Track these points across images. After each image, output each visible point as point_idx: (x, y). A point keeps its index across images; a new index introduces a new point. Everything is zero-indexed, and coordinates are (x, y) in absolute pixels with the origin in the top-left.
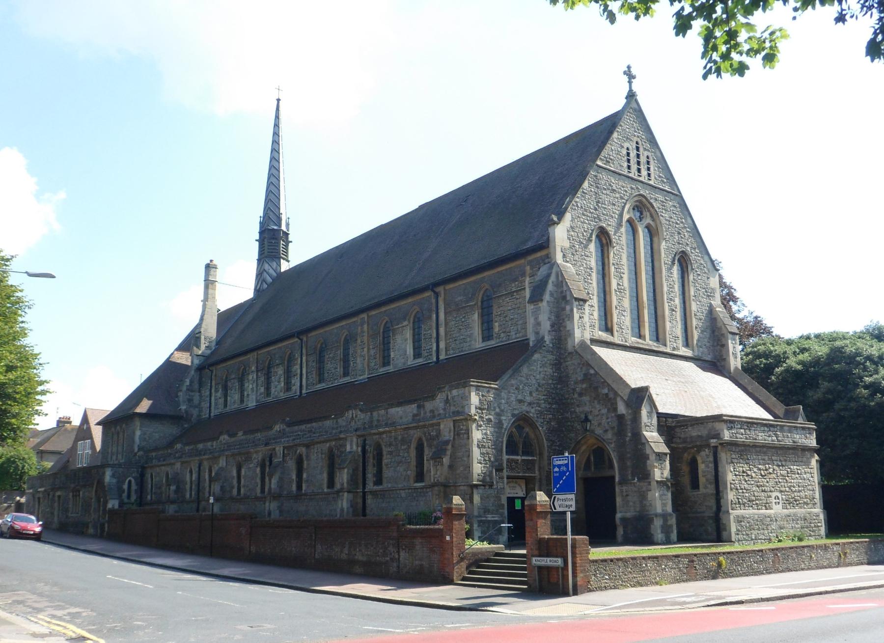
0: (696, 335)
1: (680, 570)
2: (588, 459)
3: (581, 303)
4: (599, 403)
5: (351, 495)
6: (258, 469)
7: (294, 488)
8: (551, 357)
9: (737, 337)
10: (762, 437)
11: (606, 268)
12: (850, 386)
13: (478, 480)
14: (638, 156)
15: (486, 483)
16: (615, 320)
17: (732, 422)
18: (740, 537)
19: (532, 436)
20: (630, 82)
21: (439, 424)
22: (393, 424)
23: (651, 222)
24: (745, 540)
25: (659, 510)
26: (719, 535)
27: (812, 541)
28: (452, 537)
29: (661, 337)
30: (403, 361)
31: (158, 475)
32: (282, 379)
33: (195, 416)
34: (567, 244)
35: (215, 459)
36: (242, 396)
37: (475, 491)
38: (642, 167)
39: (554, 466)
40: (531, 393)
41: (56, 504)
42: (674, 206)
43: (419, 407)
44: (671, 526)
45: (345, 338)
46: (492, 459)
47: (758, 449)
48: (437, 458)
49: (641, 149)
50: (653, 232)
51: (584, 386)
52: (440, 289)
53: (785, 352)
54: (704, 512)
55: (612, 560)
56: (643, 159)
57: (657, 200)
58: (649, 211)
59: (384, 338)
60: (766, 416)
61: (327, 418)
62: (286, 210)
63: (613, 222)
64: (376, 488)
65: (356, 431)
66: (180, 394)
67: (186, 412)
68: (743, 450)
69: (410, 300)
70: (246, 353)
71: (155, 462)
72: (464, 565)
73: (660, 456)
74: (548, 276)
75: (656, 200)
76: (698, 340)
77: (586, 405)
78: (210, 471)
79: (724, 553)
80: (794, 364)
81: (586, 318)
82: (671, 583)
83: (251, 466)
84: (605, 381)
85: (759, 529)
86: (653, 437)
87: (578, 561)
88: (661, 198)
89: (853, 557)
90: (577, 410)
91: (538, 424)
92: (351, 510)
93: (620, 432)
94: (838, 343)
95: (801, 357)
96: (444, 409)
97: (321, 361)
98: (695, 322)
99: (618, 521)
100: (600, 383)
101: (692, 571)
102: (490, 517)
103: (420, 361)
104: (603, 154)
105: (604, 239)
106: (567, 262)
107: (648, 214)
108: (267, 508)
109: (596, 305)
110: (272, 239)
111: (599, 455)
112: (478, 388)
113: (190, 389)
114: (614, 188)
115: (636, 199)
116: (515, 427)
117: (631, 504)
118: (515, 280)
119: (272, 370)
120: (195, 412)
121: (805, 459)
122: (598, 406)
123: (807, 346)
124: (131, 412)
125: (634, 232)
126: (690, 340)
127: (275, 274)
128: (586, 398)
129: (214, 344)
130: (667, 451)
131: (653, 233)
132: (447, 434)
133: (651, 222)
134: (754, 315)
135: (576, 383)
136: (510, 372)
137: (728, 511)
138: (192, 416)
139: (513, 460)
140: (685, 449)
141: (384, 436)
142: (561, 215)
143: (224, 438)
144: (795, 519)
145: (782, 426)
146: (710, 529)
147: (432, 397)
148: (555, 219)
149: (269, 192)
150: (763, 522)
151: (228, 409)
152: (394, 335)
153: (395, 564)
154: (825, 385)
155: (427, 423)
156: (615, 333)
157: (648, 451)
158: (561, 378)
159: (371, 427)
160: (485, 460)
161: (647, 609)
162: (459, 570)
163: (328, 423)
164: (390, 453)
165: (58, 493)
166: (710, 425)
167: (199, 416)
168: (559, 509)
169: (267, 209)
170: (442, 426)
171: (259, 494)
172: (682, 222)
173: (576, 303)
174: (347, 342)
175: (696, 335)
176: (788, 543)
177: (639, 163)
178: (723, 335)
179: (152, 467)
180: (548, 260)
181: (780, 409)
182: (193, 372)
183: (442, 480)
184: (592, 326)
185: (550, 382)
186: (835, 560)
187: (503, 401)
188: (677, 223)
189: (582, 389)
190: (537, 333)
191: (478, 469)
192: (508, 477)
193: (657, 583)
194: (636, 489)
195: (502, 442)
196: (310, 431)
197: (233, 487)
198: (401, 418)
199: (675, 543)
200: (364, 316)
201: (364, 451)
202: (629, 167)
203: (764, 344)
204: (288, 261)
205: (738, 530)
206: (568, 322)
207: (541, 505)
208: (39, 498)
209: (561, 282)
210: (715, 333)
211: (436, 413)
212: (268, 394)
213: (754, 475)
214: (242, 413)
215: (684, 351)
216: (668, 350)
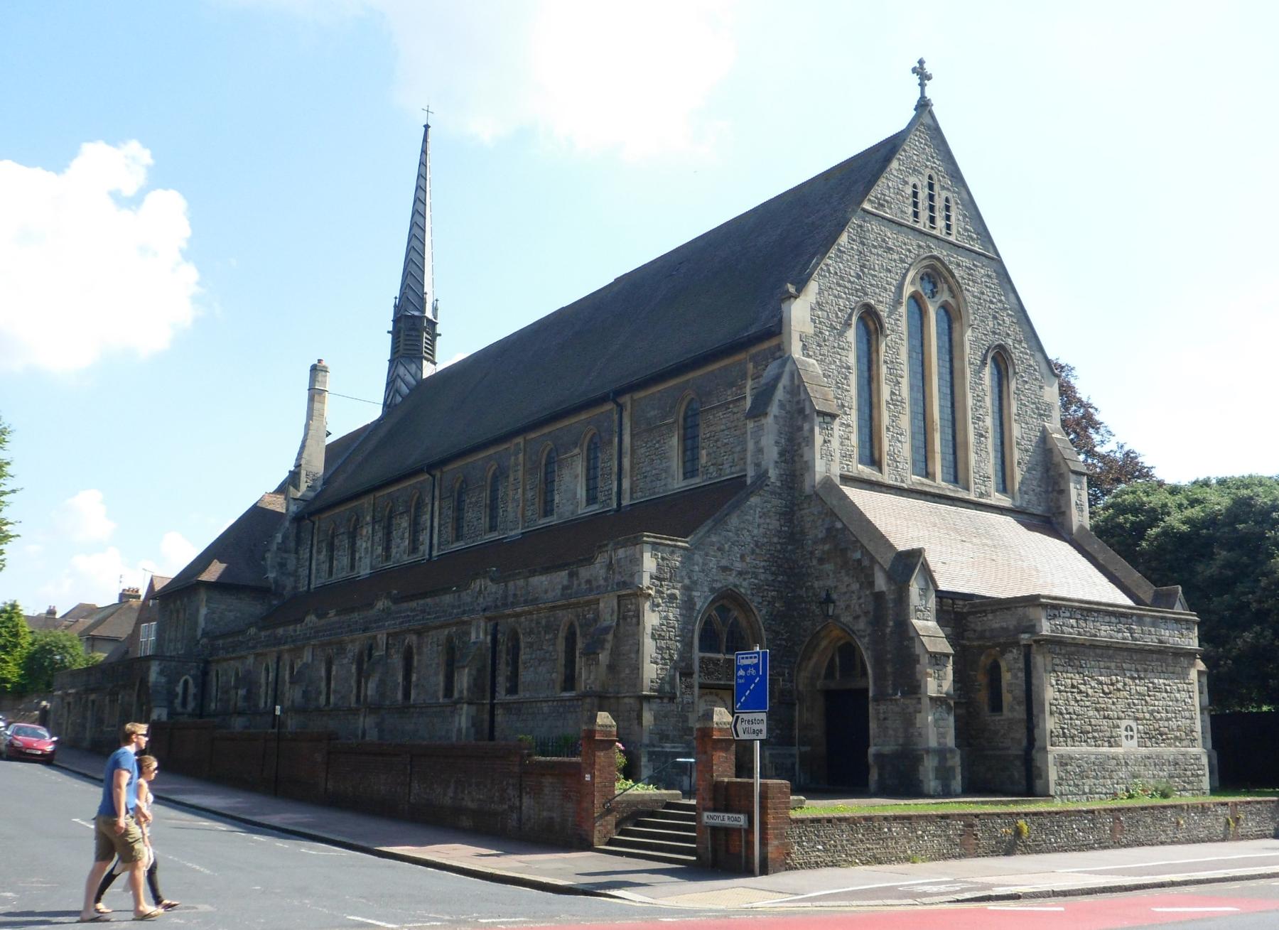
0: (1018, 475)
1: (948, 838)
2: (832, 659)
3: (828, 419)
4: (848, 574)
5: (474, 708)
6: (354, 667)
7: (400, 696)
8: (776, 502)
9: (1085, 479)
10: (1105, 632)
11: (874, 367)
12: (1261, 557)
13: (651, 689)
14: (931, 197)
15: (664, 694)
17: (1055, 607)
18: (1065, 788)
19: (743, 622)
20: (922, 85)
21: (597, 602)
22: (535, 601)
23: (950, 300)
24: (1072, 793)
25: (933, 743)
26: (1029, 783)
27: (1187, 799)
28: (593, 777)
29: (961, 475)
30: (571, 507)
31: (226, 671)
32: (407, 535)
33: (289, 588)
34: (810, 329)
35: (297, 651)
36: (353, 559)
37: (645, 706)
38: (937, 214)
39: (739, 667)
40: (742, 557)
41: (89, 714)
42: (989, 276)
43: (571, 575)
44: (952, 769)
45: (494, 473)
46: (675, 657)
47: (1098, 651)
48: (591, 652)
49: (937, 187)
50: (952, 316)
51: (827, 547)
52: (626, 399)
53: (1165, 505)
54: (1008, 748)
55: (829, 821)
56: (939, 203)
57: (959, 266)
58: (947, 282)
59: (546, 474)
60: (1122, 599)
61: (446, 590)
62: (432, 288)
63: (887, 297)
64: (508, 697)
65: (484, 610)
66: (268, 555)
67: (276, 581)
68: (1074, 653)
69: (583, 416)
70: (357, 496)
71: (222, 654)
72: (611, 819)
73: (938, 659)
74: (778, 378)
75: (958, 265)
76: (1022, 483)
77: (829, 578)
78: (292, 668)
79: (1026, 814)
80: (1177, 524)
81: (835, 443)
83: (345, 661)
84: (858, 541)
85: (1096, 778)
86: (927, 628)
87: (771, 819)
88: (966, 262)
89: (1251, 825)
90: (816, 584)
91: (753, 606)
92: (473, 730)
93: (877, 620)
94: (1245, 492)
95: (1189, 512)
96: (606, 579)
97: (459, 508)
98: (1017, 455)
99: (871, 760)
100: (852, 542)
101: (968, 840)
102: (668, 747)
103: (595, 508)
104: (873, 193)
105: (871, 324)
106: (809, 356)
107: (945, 286)
108: (361, 725)
109: (855, 425)
110: (411, 329)
111: (848, 654)
113: (283, 548)
115: (926, 263)
116: (716, 609)
117: (891, 732)
118: (732, 385)
119: (394, 522)
120: (289, 582)
121: (1178, 669)
122: (846, 579)
123: (1200, 497)
124: (193, 581)
125: (922, 313)
126: (1008, 483)
127: (414, 383)
128: (828, 567)
129: (320, 483)
130: (950, 650)
131: (951, 316)
132: (608, 617)
133: (950, 300)
134: (1126, 449)
135: (815, 543)
136: (710, 523)
137: (1045, 748)
138: (284, 588)
139: (710, 659)
140: (981, 649)
141: (523, 619)
142: (801, 285)
143: (311, 619)
144: (1159, 762)
145: (1140, 616)
146: (1016, 775)
147: (589, 560)
148: (792, 289)
149: (408, 261)
150: (1103, 767)
151: (334, 579)
152: (560, 468)
153: (515, 816)
154: (1223, 555)
155: (582, 600)
156: (885, 468)
157: (918, 650)
158: (792, 534)
159: (505, 605)
160: (663, 658)
161: (854, 903)
162: (603, 828)
163: (447, 599)
164: (531, 645)
165: (93, 697)
166: (1020, 611)
167: (295, 588)
168: (743, 736)
169: (405, 286)
170: (602, 605)
171: (353, 705)
172: (1000, 301)
173: (818, 420)
174: (495, 478)
175: (1018, 475)
176: (1147, 801)
177: (932, 208)
178: (1061, 475)
179: (218, 662)
180: (780, 354)
181: (1147, 591)
182: (287, 524)
183: (597, 688)
184: (846, 456)
186: (1220, 829)
187: (696, 568)
188: (991, 302)
189: (824, 552)
190: (758, 465)
191: (651, 672)
192: (702, 686)
193: (908, 859)
194: (897, 709)
195: (693, 631)
196: (423, 611)
197: (320, 693)
198: (546, 592)
199: (957, 796)
200: (520, 440)
201: (495, 641)
202: (916, 214)
203: (1133, 492)
204: (435, 363)
205: (1061, 779)
206: (806, 449)
207: (720, 730)
208: (69, 704)
209: (797, 388)
210: (1050, 472)
211: (595, 584)
212: (388, 557)
213: (1090, 691)
214: (351, 583)
216: (972, 497)
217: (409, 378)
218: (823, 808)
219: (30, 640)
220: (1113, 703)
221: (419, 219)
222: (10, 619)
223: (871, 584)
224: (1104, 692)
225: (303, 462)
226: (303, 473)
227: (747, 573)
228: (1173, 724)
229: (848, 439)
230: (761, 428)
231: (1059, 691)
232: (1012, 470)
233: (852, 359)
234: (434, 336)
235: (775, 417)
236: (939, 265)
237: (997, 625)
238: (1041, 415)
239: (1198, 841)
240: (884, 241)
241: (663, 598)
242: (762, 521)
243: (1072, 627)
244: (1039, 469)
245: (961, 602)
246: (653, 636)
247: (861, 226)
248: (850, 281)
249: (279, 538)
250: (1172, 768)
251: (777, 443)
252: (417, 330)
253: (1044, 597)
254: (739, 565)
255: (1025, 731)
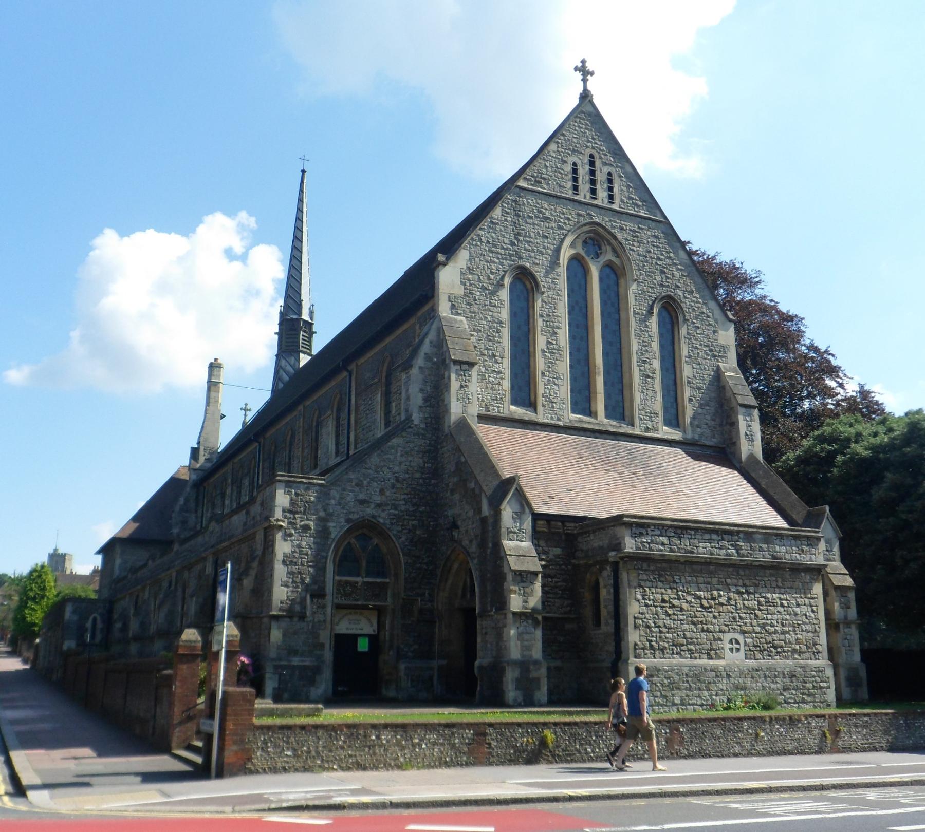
0: (689, 411)
1: (453, 746)
3: (465, 367)
8: (421, 442)
13: (280, 610)
14: (592, 173)
15: (294, 613)
16: (541, 389)
20: (585, 81)
23: (614, 259)
30: (326, 460)
34: (459, 291)
38: (598, 187)
40: (382, 492)
42: (656, 237)
43: (248, 513)
46: (307, 580)
49: (598, 164)
56: (601, 177)
57: (622, 231)
58: (610, 244)
63: (544, 260)
66: (173, 515)
73: (524, 577)
75: (622, 229)
76: (693, 418)
82: (429, 767)
85: (690, 689)
87: (230, 725)
88: (630, 225)
89: (856, 738)
98: (687, 392)
105: (525, 284)
107: (609, 248)
112: (288, 484)
113: (185, 509)
114: (548, 214)
115: (586, 228)
127: (292, 371)
128: (457, 497)
133: (614, 259)
139: (347, 582)
144: (771, 674)
156: (540, 409)
157: (506, 570)
160: (294, 582)
172: (670, 258)
173: (454, 368)
176: (746, 713)
177: (593, 182)
178: (732, 409)
180: (433, 314)
181: (800, 510)
182: (188, 489)
185: (418, 475)
186: (813, 742)
188: (659, 259)
190: (407, 411)
191: (281, 593)
202: (576, 188)
209: (440, 344)
213: (685, 606)
215: (666, 432)
217: (289, 368)
218: (421, 714)
219: (55, 593)
220: (715, 617)
221: (297, 244)
222: (39, 576)
223: (479, 510)
224: (702, 606)
225: (201, 440)
226: (202, 448)
227: (387, 505)
228: (791, 637)
229: (499, 384)
230: (409, 378)
231: (647, 605)
232: (683, 406)
233: (505, 314)
234: (311, 333)
235: (420, 368)
236: (600, 229)
237: (596, 545)
238: (715, 356)
239: (785, 754)
240: (540, 212)
241: (295, 529)
242: (404, 459)
243: (663, 544)
244: (712, 404)
245: (572, 525)
246: (284, 563)
247: (515, 201)
248: (503, 248)
249: (182, 501)
250: (788, 680)
251: (422, 390)
252: (295, 330)
253: (628, 516)
254: (377, 499)
255: (613, 644)
